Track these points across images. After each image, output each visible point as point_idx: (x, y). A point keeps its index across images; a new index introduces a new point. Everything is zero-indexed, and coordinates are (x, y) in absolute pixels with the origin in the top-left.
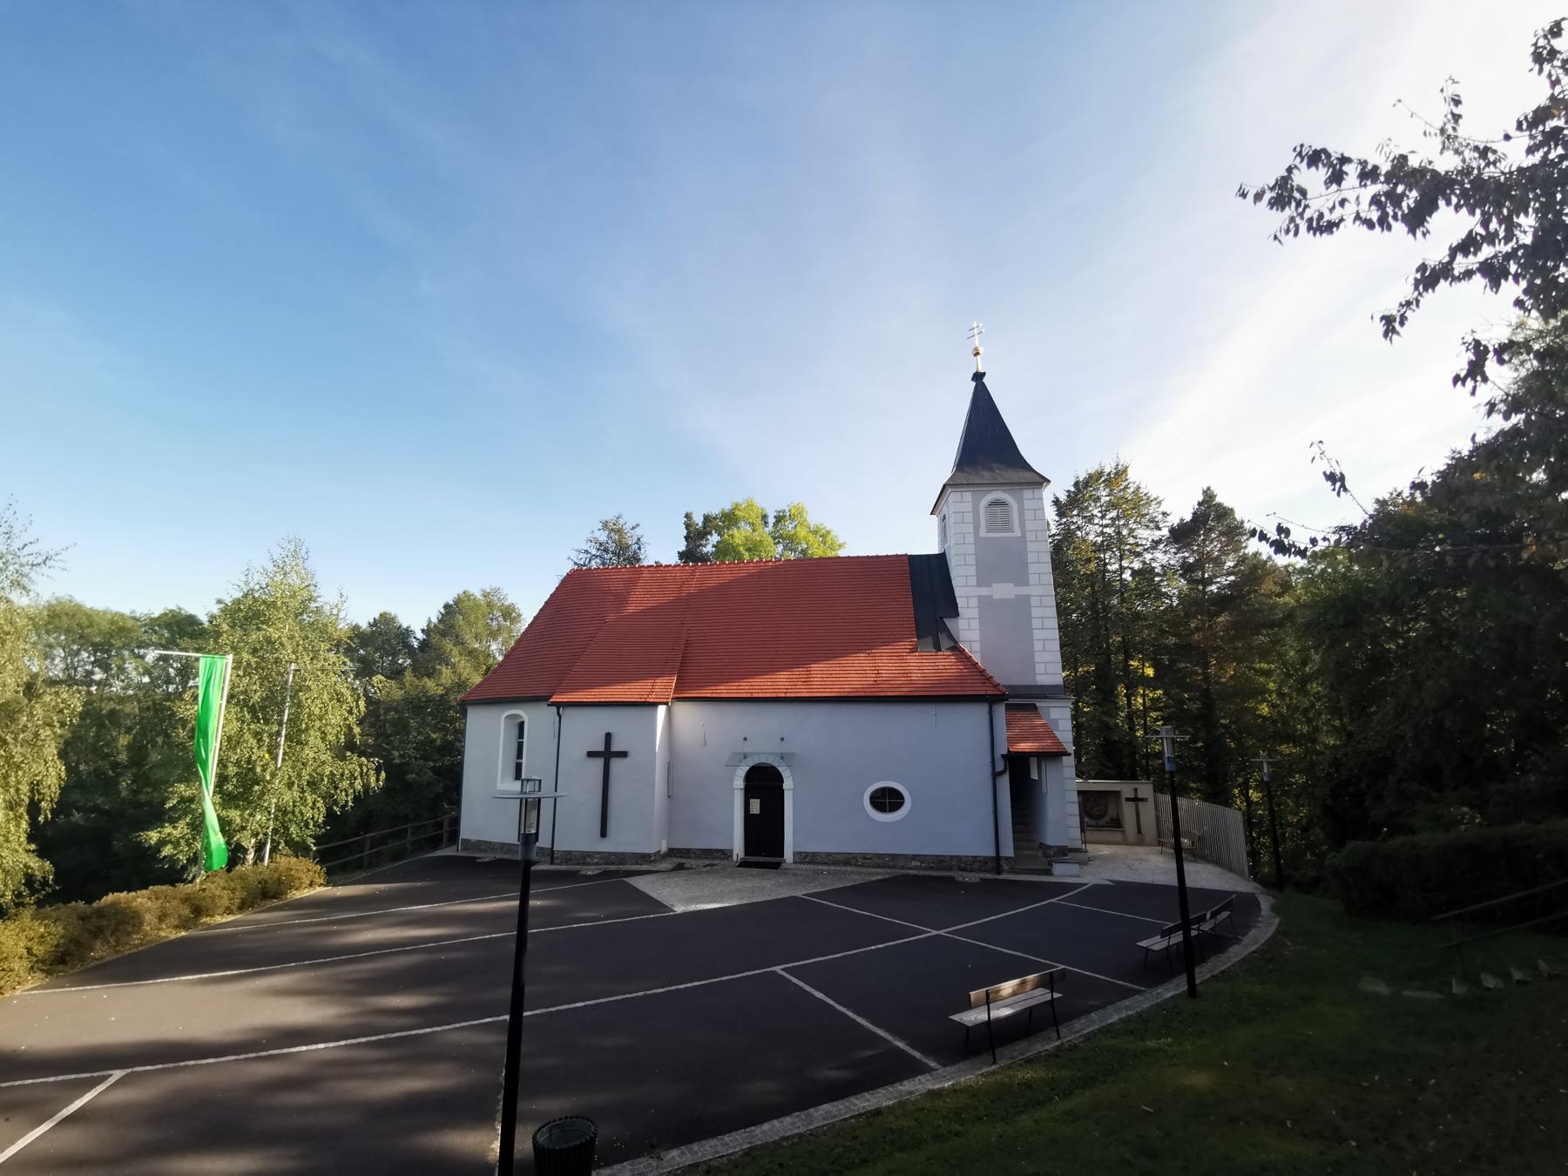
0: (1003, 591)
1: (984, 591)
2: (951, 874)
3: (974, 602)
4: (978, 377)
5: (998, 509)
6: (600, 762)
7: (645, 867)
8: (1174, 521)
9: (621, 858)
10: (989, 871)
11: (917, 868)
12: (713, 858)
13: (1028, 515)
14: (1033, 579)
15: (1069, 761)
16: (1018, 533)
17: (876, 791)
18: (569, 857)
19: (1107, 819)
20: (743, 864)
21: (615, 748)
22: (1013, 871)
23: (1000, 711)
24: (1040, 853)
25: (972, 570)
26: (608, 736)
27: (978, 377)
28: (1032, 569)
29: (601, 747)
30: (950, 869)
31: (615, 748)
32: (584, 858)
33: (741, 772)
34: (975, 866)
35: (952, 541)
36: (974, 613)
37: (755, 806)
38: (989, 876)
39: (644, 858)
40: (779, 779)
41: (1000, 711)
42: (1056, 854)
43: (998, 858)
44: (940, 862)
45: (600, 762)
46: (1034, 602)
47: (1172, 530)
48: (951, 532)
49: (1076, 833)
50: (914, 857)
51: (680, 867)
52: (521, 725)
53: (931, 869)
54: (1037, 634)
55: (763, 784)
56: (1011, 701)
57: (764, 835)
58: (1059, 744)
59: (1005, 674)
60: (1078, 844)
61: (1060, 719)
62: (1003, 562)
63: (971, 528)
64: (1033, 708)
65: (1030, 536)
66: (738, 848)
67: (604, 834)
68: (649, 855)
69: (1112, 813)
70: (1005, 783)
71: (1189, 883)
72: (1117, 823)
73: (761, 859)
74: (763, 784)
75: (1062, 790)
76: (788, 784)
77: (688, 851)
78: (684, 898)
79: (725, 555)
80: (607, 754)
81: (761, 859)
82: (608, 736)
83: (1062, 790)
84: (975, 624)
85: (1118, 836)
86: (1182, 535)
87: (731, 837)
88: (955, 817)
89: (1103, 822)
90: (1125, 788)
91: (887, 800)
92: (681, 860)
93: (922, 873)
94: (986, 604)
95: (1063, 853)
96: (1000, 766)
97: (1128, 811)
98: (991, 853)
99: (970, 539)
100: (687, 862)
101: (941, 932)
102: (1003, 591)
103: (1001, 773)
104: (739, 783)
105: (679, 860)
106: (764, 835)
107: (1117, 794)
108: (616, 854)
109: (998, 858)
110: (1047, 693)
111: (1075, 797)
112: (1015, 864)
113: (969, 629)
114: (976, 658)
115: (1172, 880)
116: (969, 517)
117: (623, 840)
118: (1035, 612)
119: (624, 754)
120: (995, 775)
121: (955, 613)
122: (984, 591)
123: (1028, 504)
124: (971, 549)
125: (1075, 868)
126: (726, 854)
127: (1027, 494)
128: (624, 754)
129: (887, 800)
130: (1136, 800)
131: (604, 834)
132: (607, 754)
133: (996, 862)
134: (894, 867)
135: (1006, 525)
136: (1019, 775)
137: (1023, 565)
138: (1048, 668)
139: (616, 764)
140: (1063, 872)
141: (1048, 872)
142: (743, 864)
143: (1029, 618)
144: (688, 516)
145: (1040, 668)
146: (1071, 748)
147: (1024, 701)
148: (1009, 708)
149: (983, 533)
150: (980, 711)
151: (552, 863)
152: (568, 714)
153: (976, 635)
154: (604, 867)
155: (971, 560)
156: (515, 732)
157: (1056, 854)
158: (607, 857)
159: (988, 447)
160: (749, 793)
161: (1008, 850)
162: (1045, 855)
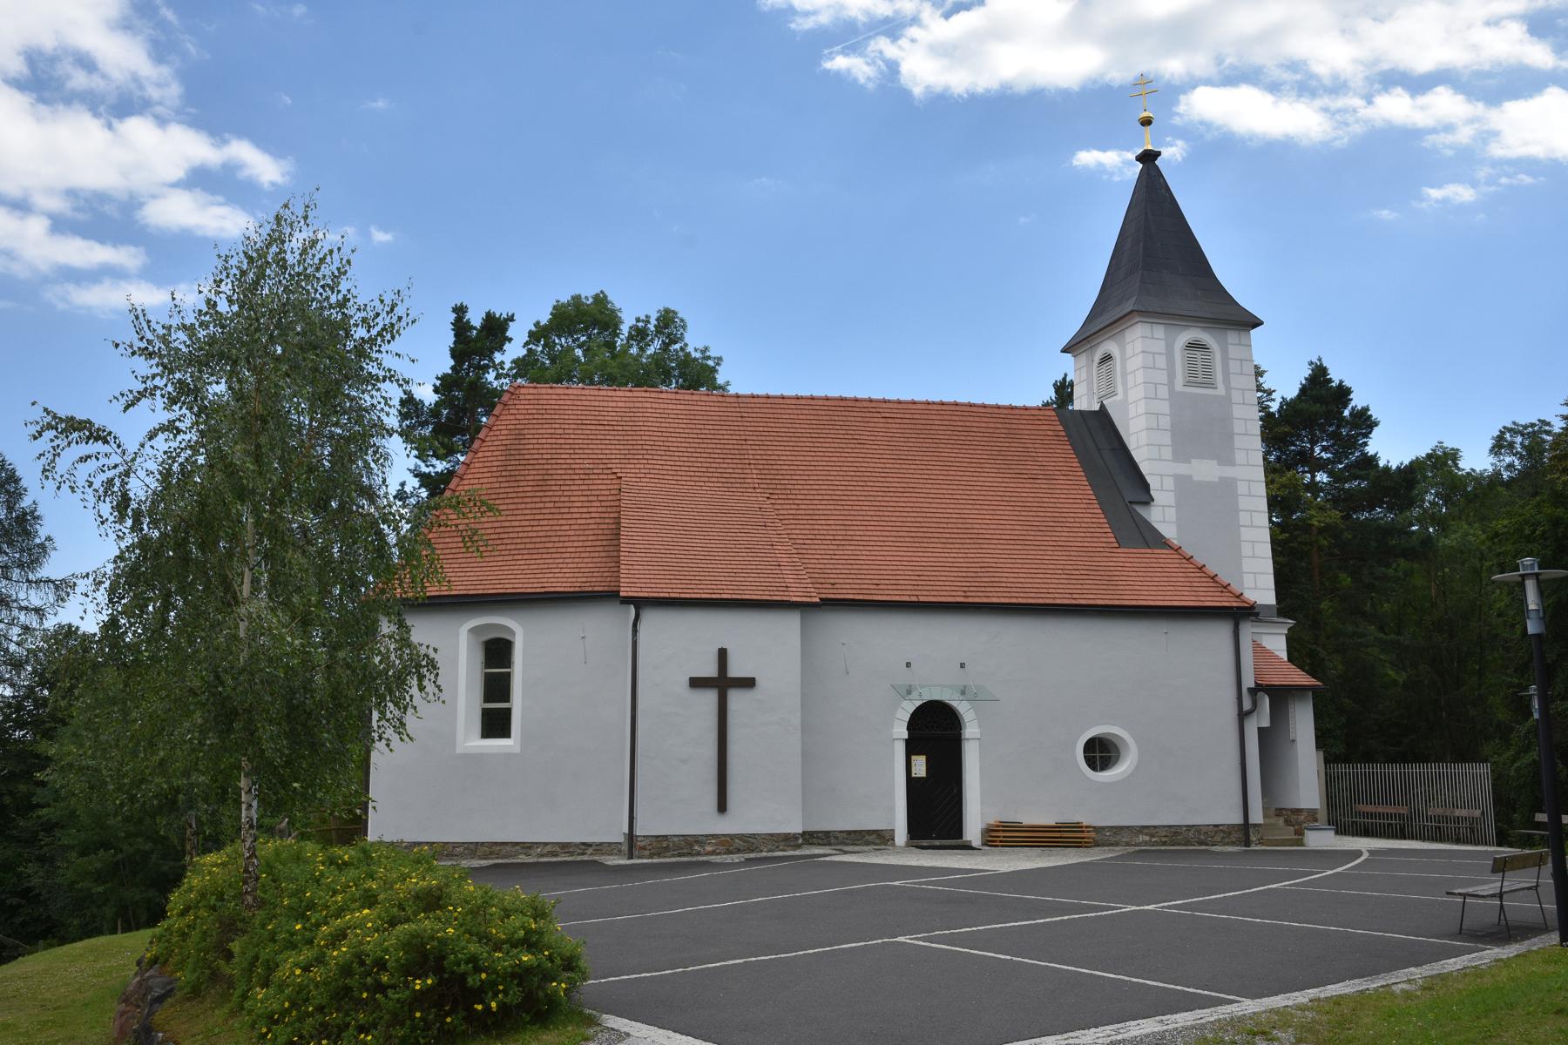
3: (1169, 483)
4: (1148, 158)
5: (1199, 354)
10: (1233, 844)
11: (1146, 843)
14: (1240, 457)
21: (734, 671)
24: (1281, 821)
26: (723, 654)
27: (1148, 158)
28: (1239, 442)
31: (734, 671)
33: (909, 707)
37: (920, 767)
43: (1246, 826)
45: (710, 697)
46: (1242, 488)
50: (1142, 829)
53: (1164, 844)
55: (935, 731)
57: (935, 810)
63: (1162, 377)
67: (722, 807)
68: (795, 837)
71: (638, 832)
74: (935, 731)
76: (971, 730)
77: (827, 833)
79: (243, 488)
80: (722, 683)
82: (723, 654)
94: (1182, 483)
98: (1237, 819)
99: (1163, 392)
102: (1205, 470)
106: (935, 810)
109: (1246, 826)
116: (1161, 362)
119: (749, 683)
121: (1148, 500)
123: (1234, 351)
124: (1165, 407)
127: (1232, 337)
128: (749, 683)
129: (1100, 753)
131: (722, 807)
132: (722, 683)
134: (1117, 844)
139: (736, 698)
141: (1300, 843)
145: (1248, 581)
152: (653, 621)
160: (913, 747)
161: (1257, 817)
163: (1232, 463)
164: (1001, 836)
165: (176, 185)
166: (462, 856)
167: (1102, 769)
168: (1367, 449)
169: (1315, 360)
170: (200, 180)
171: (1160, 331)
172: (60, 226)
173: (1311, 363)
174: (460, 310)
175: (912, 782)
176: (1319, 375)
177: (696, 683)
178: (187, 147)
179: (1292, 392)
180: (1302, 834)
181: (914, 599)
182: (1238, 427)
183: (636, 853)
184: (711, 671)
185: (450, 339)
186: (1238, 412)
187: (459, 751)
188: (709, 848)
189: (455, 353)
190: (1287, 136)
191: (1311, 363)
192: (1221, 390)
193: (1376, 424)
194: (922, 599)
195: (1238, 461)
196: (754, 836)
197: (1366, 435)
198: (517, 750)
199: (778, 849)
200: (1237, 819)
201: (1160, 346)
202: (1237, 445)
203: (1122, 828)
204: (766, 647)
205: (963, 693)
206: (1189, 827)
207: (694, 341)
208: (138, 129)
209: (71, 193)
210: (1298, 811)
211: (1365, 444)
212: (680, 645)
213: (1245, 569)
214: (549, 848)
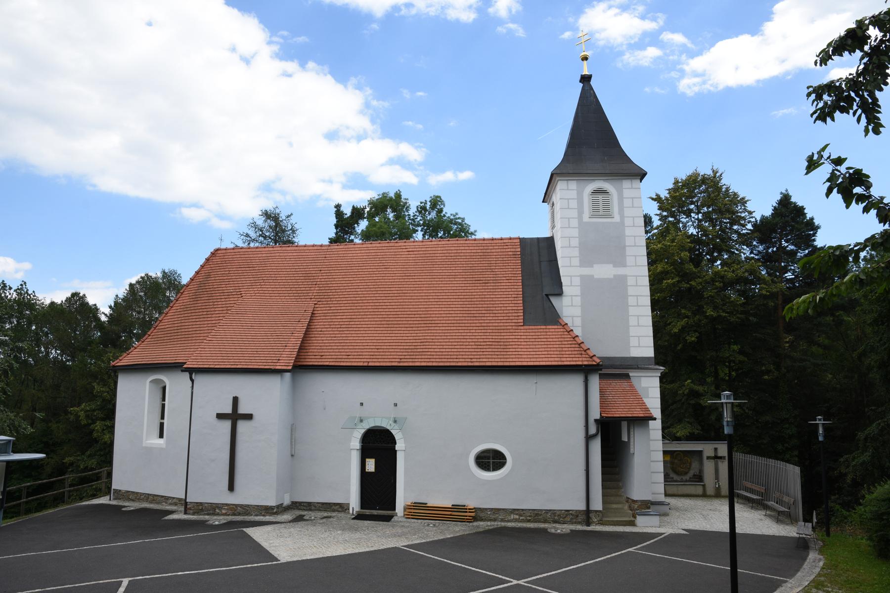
0: (604, 271)
1: (586, 271)
2: (542, 525)
3: (577, 281)
4: (586, 79)
5: (600, 197)
6: (227, 424)
7: (268, 518)
8: (758, 216)
9: (246, 509)
10: (579, 523)
12: (332, 509)
13: (627, 203)
14: (630, 261)
15: (656, 426)
16: (617, 218)
18: (200, 508)
19: (691, 473)
20: (359, 517)
21: (242, 410)
22: (601, 523)
23: (595, 382)
24: (626, 507)
25: (576, 252)
26: (236, 400)
27: (586, 79)
28: (629, 251)
29: (228, 410)
30: (545, 521)
31: (242, 410)
32: (213, 509)
33: (358, 434)
35: (558, 224)
36: (577, 291)
37: (371, 465)
38: (579, 527)
39: (267, 510)
40: (391, 440)
41: (595, 382)
42: (640, 507)
44: (536, 515)
45: (227, 424)
46: (631, 281)
47: (755, 225)
48: (558, 216)
49: (661, 488)
50: (514, 511)
51: (299, 519)
52: (164, 388)
53: (529, 521)
54: (632, 311)
55: (379, 444)
56: (604, 371)
57: (378, 493)
58: (647, 409)
59: (603, 348)
60: (662, 498)
61: (649, 389)
62: (602, 246)
63: (575, 213)
64: (627, 377)
65: (628, 222)
66: (354, 502)
68: (271, 508)
70: (596, 447)
72: (699, 478)
73: (375, 512)
74: (379, 444)
75: (648, 451)
77: (309, 504)
78: (285, 544)
80: (235, 416)
81: (375, 512)
82: (236, 400)
83: (648, 451)
84: (578, 301)
85: (699, 490)
86: (765, 230)
87: (348, 491)
88: (550, 471)
89: (687, 477)
90: (707, 448)
91: (491, 460)
92: (300, 511)
93: (520, 525)
94: (587, 283)
95: (646, 506)
96: (593, 430)
97: (709, 467)
98: (582, 507)
99: (575, 223)
100: (307, 514)
101: (521, 582)
102: (604, 271)
103: (594, 436)
104: (356, 444)
105: (299, 513)
106: (378, 493)
108: (241, 506)
110: (638, 364)
111: (660, 456)
113: (570, 307)
114: (578, 331)
115: (725, 528)
116: (574, 204)
117: (245, 496)
118: (631, 291)
119: (249, 417)
120: (588, 438)
121: (560, 294)
122: (586, 271)
123: (627, 193)
124: (575, 233)
125: (655, 520)
126: (342, 508)
127: (626, 183)
128: (249, 417)
129: (491, 460)
130: (716, 458)
132: (235, 416)
133: (587, 515)
134: (495, 520)
135: (608, 213)
136: (611, 437)
137: (621, 249)
138: (641, 342)
139: (242, 425)
140: (646, 524)
141: (632, 524)
142: (359, 517)
143: (625, 296)
145: (633, 342)
146: (657, 413)
147: (614, 370)
148: (603, 377)
149: (586, 218)
151: (185, 513)
152: (200, 379)
153: (577, 311)
154: (230, 518)
155: (575, 242)
156: (160, 395)
157: (640, 507)
158: (234, 509)
159: (594, 148)
160: (366, 452)
161: (597, 504)
162: (631, 508)
163: (624, 265)
164: (418, 511)
165: (382, 165)
166: (143, 500)
167: (494, 470)
168: (816, 243)
169: (784, 192)
170: (392, 162)
171: (573, 185)
172: (345, 187)
173: (781, 193)
174: (338, 207)
175: (364, 475)
176: (785, 201)
177: (220, 416)
178: (385, 149)
179: (768, 212)
180: (635, 517)
181: (366, 364)
182: (629, 242)
183: (188, 511)
184: (228, 410)
185: (334, 221)
186: (628, 232)
187: (144, 445)
188: (224, 511)
189: (336, 226)
190: (347, 4)
191: (781, 193)
192: (617, 218)
193: (818, 227)
194: (370, 364)
195: (628, 264)
196: (248, 506)
197: (814, 235)
198: (164, 446)
199: (261, 515)
200: (582, 507)
201: (574, 194)
202: (627, 253)
203: (499, 510)
204: (264, 397)
205: (395, 422)
206: (547, 511)
207: (449, 211)
208: (366, 144)
209: (345, 174)
210: (634, 501)
211: (814, 240)
212: (216, 393)
213: (631, 334)
214: (174, 500)
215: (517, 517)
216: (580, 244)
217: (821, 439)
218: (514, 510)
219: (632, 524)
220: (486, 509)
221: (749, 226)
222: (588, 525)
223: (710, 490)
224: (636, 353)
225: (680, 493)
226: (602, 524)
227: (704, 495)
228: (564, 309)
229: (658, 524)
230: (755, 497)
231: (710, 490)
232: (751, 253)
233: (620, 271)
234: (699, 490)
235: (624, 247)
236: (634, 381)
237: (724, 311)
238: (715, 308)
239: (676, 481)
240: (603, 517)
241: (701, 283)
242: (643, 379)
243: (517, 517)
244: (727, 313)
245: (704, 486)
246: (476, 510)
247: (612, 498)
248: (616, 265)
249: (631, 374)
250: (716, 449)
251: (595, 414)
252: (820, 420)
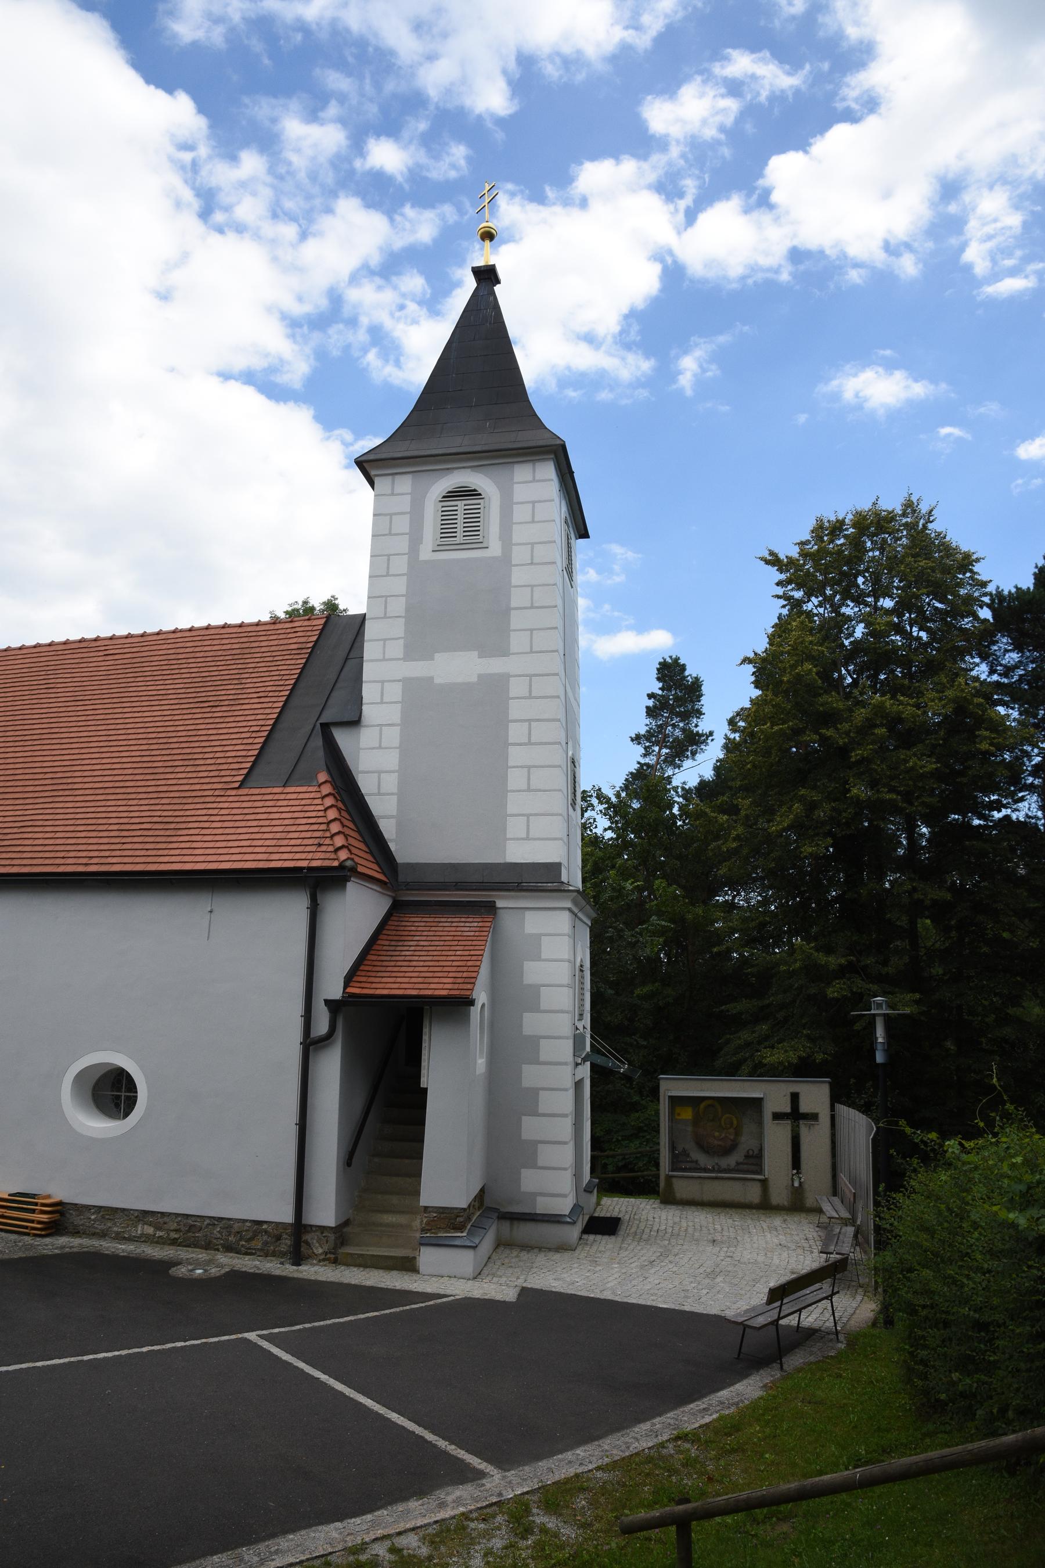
0: (457, 667)
1: (417, 669)
5: (461, 505)
13: (520, 513)
17: (129, 1076)
22: (334, 1260)
34: (257, 1244)
36: (392, 713)
43: (299, 1228)
46: (396, 649)
50: (144, 1215)
63: (402, 544)
64: (490, 908)
65: (519, 554)
69: (747, 1142)
70: (330, 1066)
84: (393, 736)
89: (731, 1161)
91: (113, 1091)
94: (418, 695)
96: (321, 1025)
97: (776, 1139)
98: (285, 1215)
99: (401, 565)
103: (327, 1039)
107: (756, 1104)
109: (299, 1228)
110: (536, 880)
112: (340, 1242)
116: (402, 524)
120: (311, 1046)
121: (355, 722)
122: (417, 669)
124: (400, 586)
129: (113, 1091)
136: (383, 1044)
143: (503, 721)
144: (762, 559)
145: (515, 827)
149: (426, 553)
150: (289, 912)
153: (391, 760)
161: (324, 1211)
192: (495, 548)
195: (514, 648)
200: (285, 1215)
201: (404, 503)
203: (114, 1211)
215: (150, 1230)
216: (407, 610)
217: (880, 1058)
218: (146, 1213)
219: (409, 1265)
220: (88, 1208)
221: (985, 614)
222: (298, 1259)
223: (779, 1195)
224: (520, 852)
225: (707, 1197)
226: (335, 1262)
227: (765, 1206)
228: (363, 755)
229: (469, 1270)
230: (39, 1226)
231: (779, 1195)
232: (992, 672)
233: (496, 666)
234: (754, 1193)
235: (507, 611)
236: (507, 921)
237: (892, 790)
238: (873, 784)
239: (706, 1170)
240: (340, 1242)
241: (847, 733)
242: (529, 915)
243: (150, 1230)
244: (898, 793)
245: (764, 1183)
246: (60, 1208)
247: (395, 1200)
248: (486, 651)
249: (500, 904)
250: (795, 1097)
251: (332, 987)
252: (879, 1006)
